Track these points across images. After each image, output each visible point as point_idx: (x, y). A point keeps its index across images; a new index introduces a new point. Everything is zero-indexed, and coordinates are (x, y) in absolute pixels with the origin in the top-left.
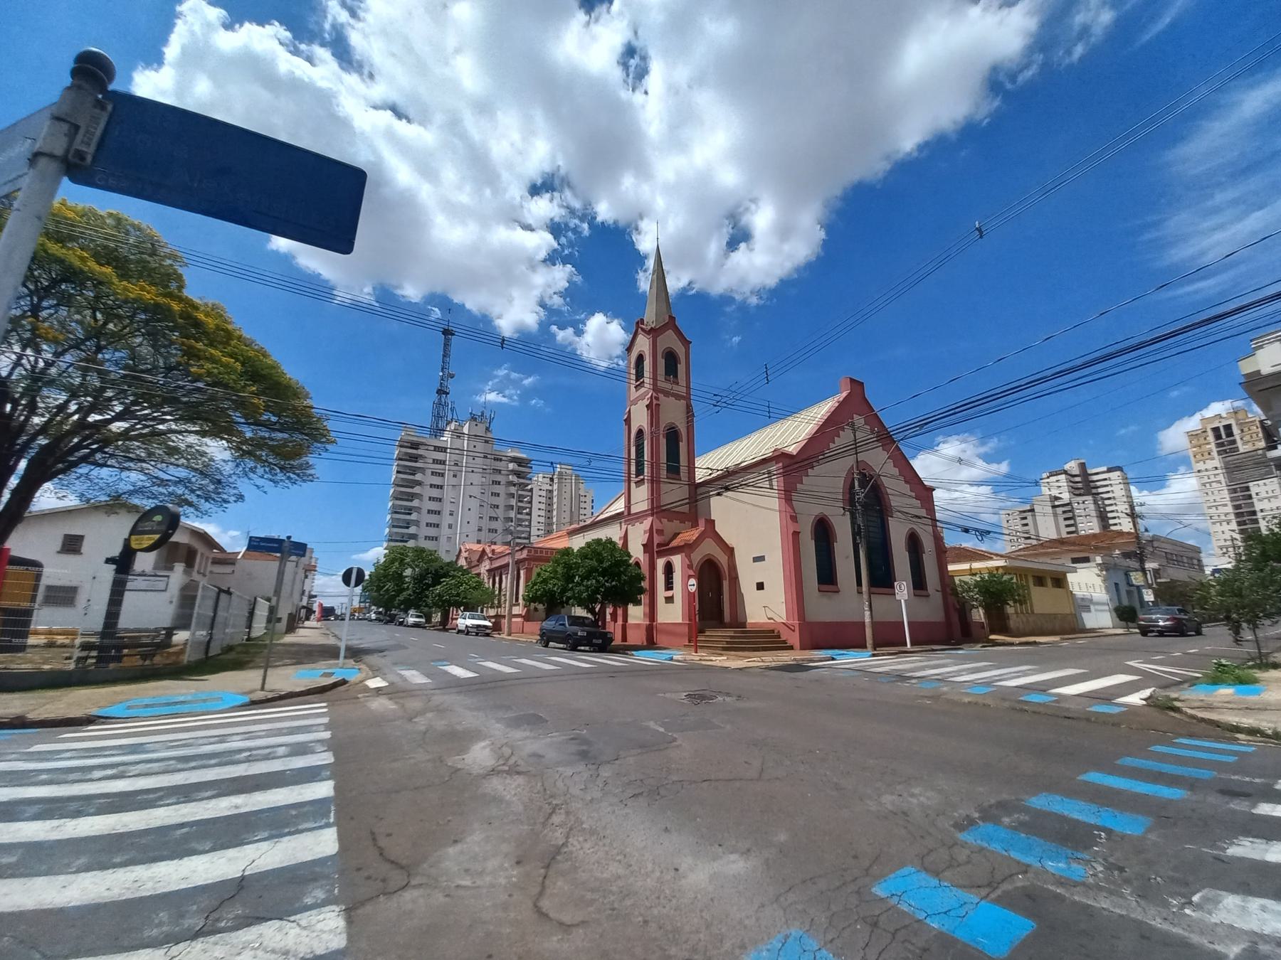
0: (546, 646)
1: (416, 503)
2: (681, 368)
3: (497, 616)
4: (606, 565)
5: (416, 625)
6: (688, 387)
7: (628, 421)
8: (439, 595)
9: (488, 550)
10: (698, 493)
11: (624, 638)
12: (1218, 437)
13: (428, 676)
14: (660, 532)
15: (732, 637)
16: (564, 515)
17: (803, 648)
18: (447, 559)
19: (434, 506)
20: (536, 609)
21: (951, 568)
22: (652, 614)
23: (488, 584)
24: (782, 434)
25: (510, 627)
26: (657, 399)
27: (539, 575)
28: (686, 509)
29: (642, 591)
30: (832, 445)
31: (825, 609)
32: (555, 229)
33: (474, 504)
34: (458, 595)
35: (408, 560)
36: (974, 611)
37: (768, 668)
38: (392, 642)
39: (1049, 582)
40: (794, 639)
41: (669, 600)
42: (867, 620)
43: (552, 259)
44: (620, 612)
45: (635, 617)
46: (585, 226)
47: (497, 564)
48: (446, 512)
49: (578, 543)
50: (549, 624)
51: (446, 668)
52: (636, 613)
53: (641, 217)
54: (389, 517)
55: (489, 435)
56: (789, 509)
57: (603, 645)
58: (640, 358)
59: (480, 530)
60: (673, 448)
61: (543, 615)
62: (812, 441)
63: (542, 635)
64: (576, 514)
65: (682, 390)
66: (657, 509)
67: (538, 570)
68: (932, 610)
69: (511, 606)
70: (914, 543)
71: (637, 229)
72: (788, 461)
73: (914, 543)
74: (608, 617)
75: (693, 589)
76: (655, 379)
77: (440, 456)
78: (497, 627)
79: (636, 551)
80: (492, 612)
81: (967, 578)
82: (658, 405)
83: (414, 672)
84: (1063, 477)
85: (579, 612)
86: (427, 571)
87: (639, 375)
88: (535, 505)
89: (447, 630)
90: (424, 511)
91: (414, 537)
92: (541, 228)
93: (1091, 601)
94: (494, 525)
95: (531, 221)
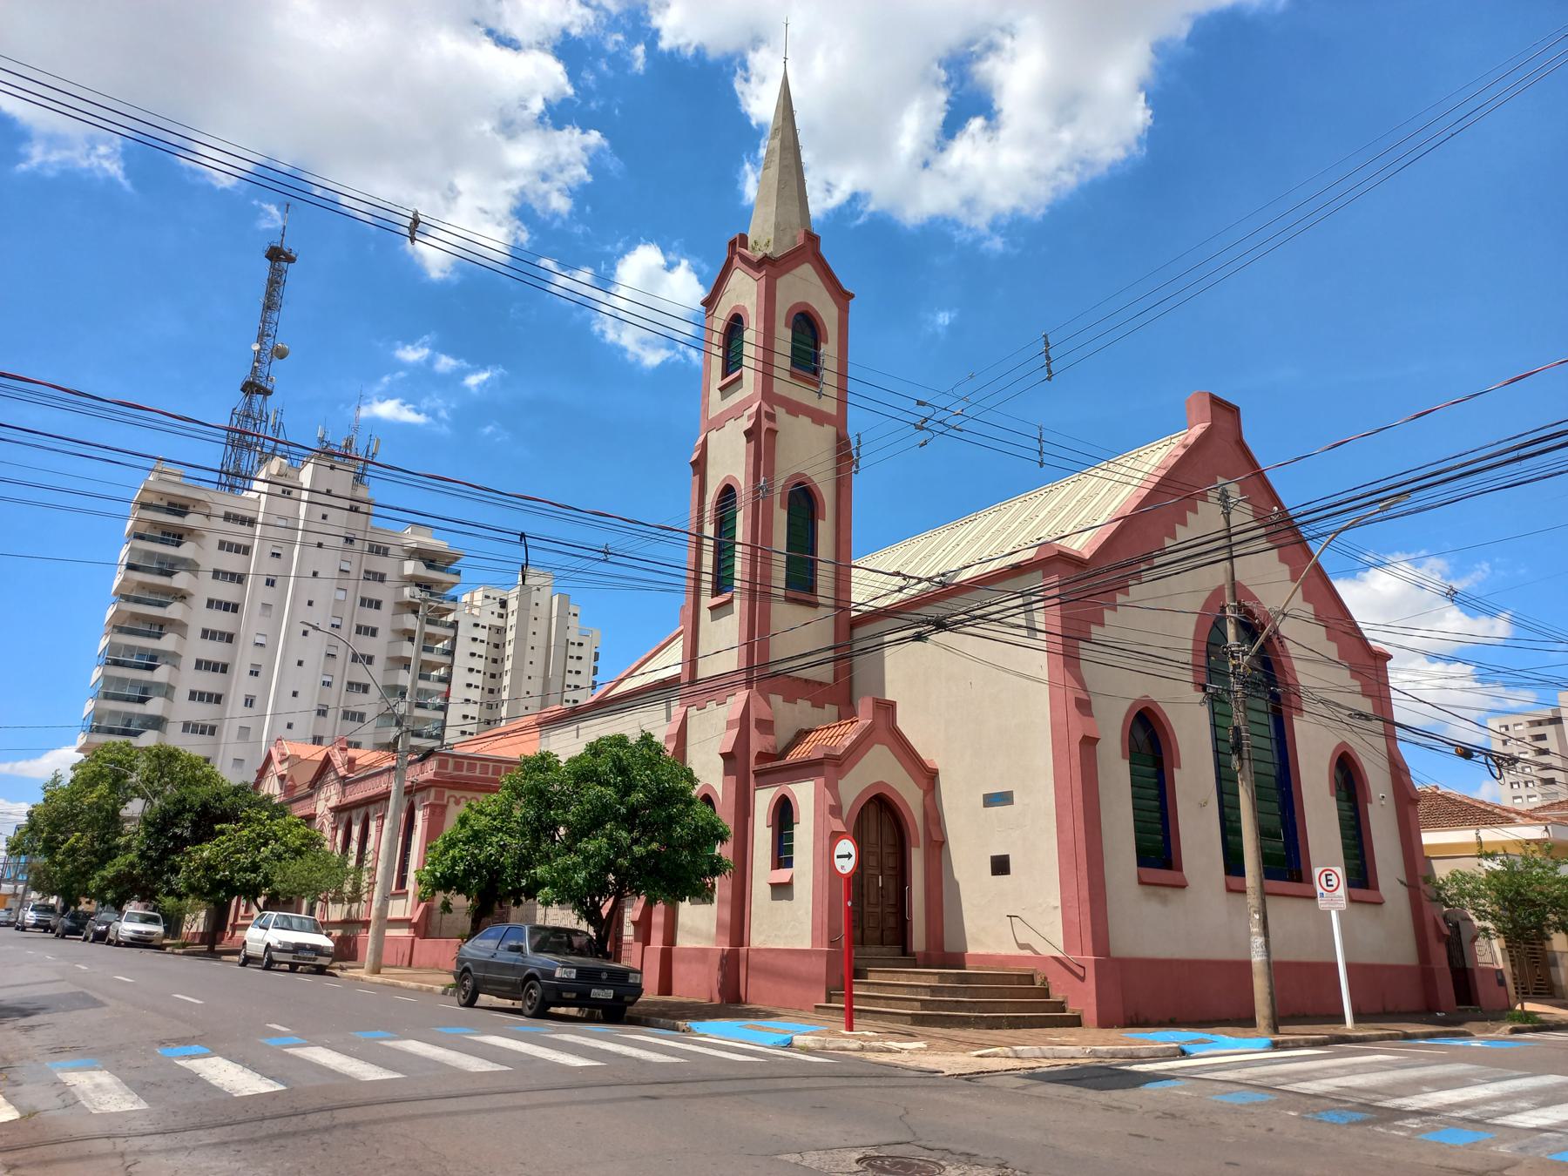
0: (470, 1003)
1: (168, 642)
2: (829, 350)
3: (347, 923)
4: (638, 796)
5: (140, 942)
6: (842, 402)
7: (700, 466)
8: (210, 867)
9: (338, 759)
10: (856, 635)
11: (666, 987)
13: (140, 1088)
14: (766, 726)
15: (933, 990)
16: (527, 686)
17: (1105, 1022)
18: (230, 775)
19: (214, 651)
20: (446, 907)
21: (1429, 838)
22: (738, 926)
23: (331, 839)
24: (1052, 514)
25: (378, 953)
26: (771, 417)
27: (463, 821)
28: (825, 673)
29: (716, 868)
30: (1168, 542)
31: (1154, 928)
32: (568, 50)
33: (315, 647)
34: (255, 867)
35: (134, 779)
36: (1481, 943)
37: (1033, 1075)
38: (66, 988)
40: (1082, 998)
41: (782, 890)
42: (1257, 958)
43: (558, 115)
44: (658, 918)
45: (694, 933)
46: (640, 50)
47: (357, 793)
48: (241, 668)
49: (567, 745)
50: (483, 947)
51: (197, 1065)
52: (698, 923)
53: (757, 42)
54: (97, 673)
55: (362, 493)
56: (1072, 683)
57: (610, 1000)
58: (735, 325)
59: (322, 713)
60: (803, 531)
61: (467, 923)
62: (1128, 526)
63: (463, 973)
64: (555, 686)
65: (830, 407)
66: (760, 672)
67: (462, 809)
68: (1390, 937)
69: (385, 900)
70: (1347, 773)
71: (745, 68)
72: (1073, 573)
73: (1347, 773)
74: (628, 931)
75: (846, 866)
76: (767, 375)
77: (237, 533)
78: (346, 951)
79: (707, 768)
80: (336, 913)
81: (1468, 866)
82: (772, 432)
83: (104, 1078)
85: (562, 917)
86: (181, 807)
87: (732, 362)
88: (462, 660)
89: (213, 954)
90: (188, 662)
91: (157, 723)
92: (540, 46)
94: (358, 702)
95: (518, 32)
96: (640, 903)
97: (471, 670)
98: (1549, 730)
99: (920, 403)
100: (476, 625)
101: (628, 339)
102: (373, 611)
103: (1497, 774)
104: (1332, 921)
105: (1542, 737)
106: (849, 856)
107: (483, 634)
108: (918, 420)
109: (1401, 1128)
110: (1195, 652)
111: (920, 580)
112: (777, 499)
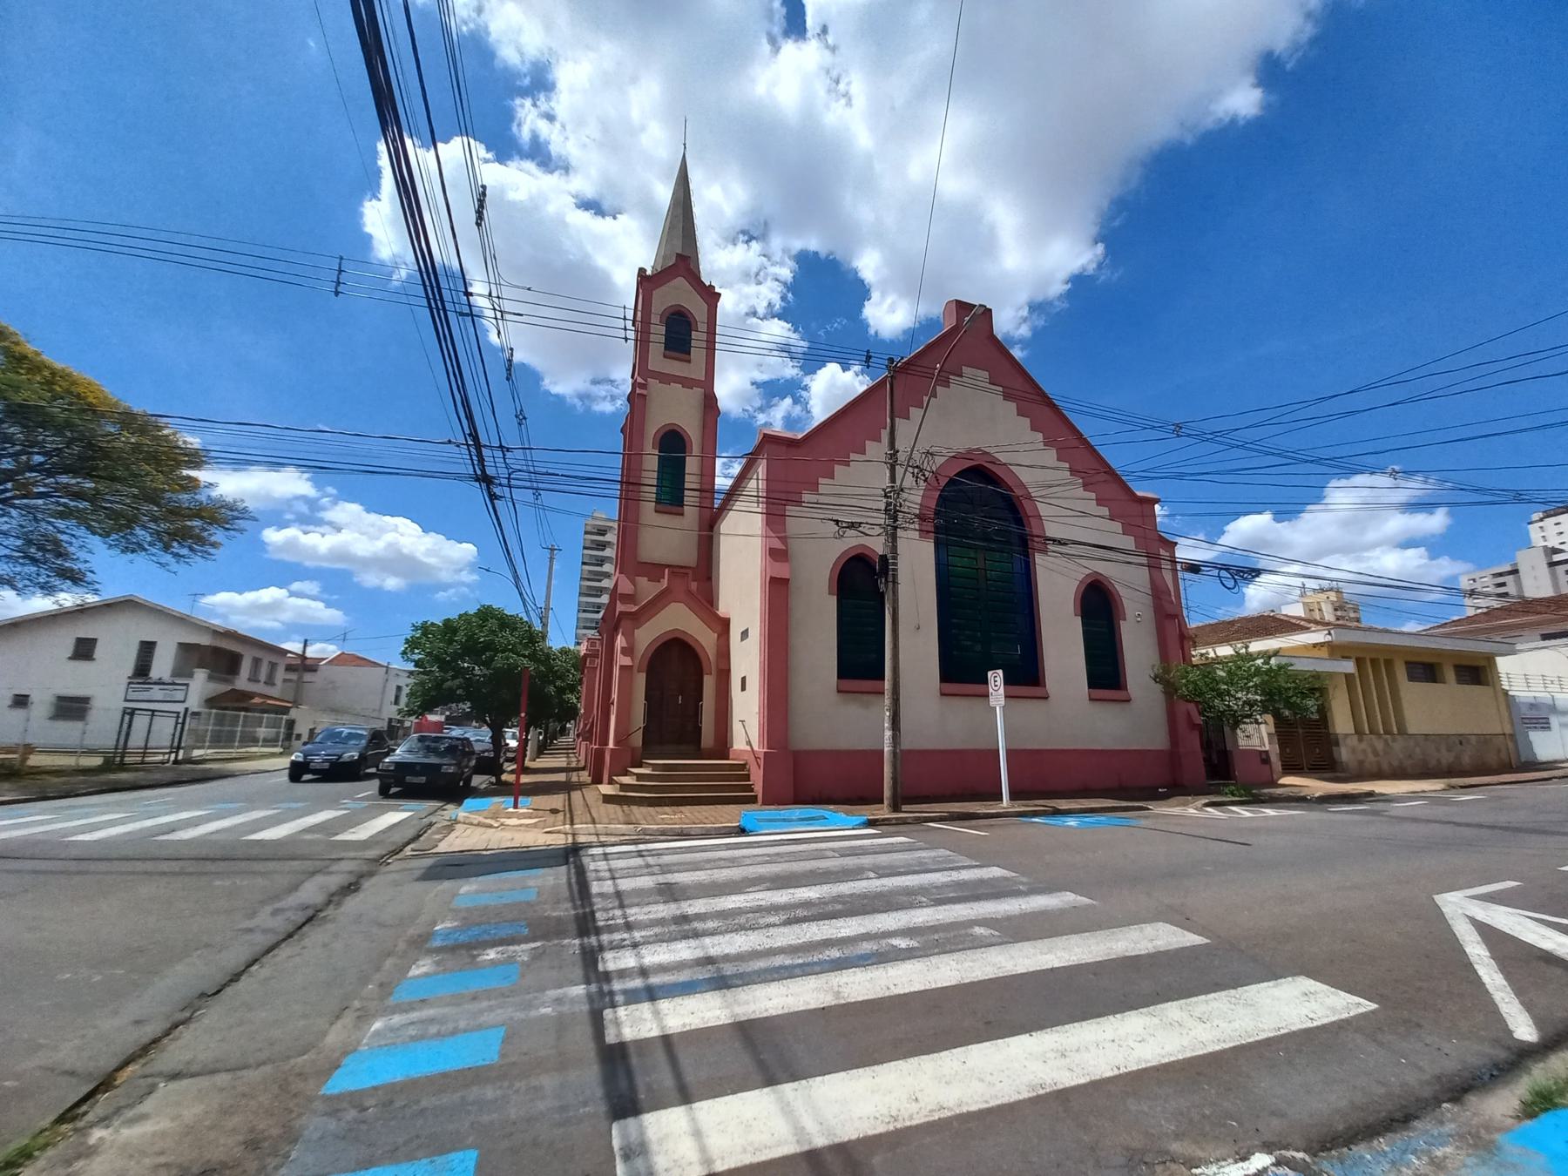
2: (698, 337)
31: (859, 725)
39: (1450, 674)
42: (887, 749)
65: (695, 370)
73: (1097, 604)
93: (1553, 708)
98: (1509, 579)
103: (1230, 583)
104: (1068, 711)
105: (1503, 584)
112: (696, 450)
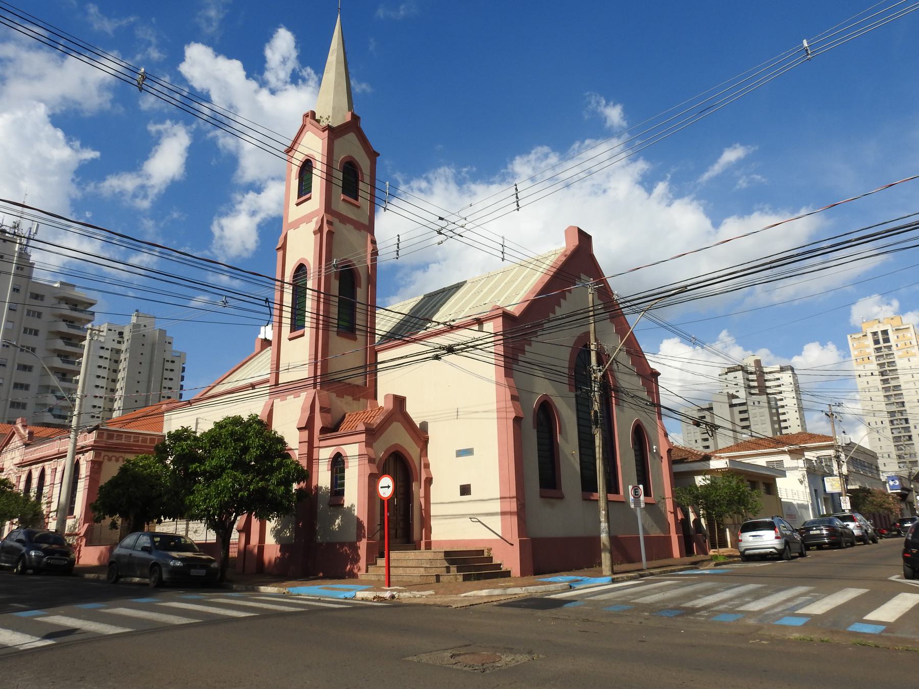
2: (364, 187)
12: (876, 342)
24: (491, 290)
31: (558, 521)
58: (306, 167)
84: (740, 374)
87: (304, 189)
96: (241, 520)
97: (98, 377)
98: (706, 413)
99: (441, 219)
100: (102, 348)
101: (588, 93)
102: (32, 337)
106: (389, 487)
107: (107, 354)
108: (437, 228)
109: (700, 616)
110: (569, 368)
111: (439, 323)
